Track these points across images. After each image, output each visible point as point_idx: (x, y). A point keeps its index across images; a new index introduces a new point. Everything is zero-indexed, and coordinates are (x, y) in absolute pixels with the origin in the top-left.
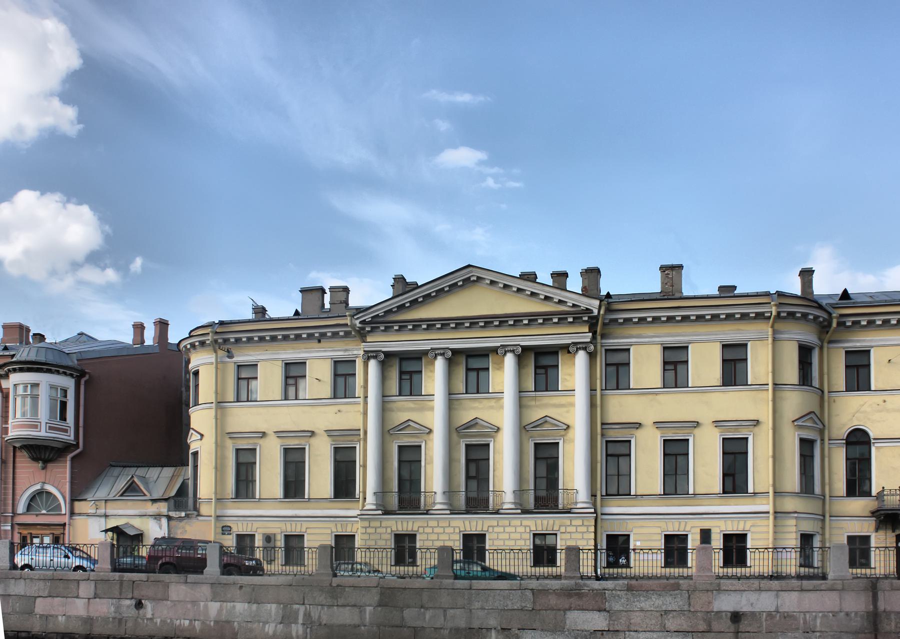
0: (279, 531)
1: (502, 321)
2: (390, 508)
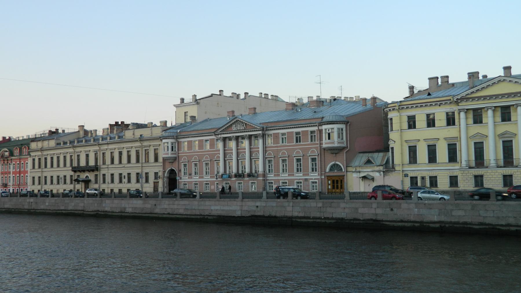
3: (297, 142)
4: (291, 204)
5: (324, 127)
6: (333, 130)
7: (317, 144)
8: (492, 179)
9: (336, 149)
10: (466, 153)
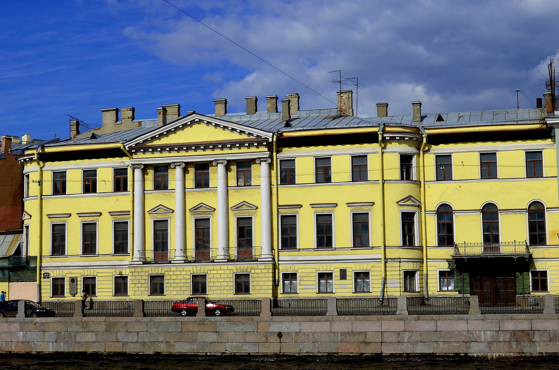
0: (80, 275)
1: (215, 145)
2: (148, 260)
8: (176, 281)
10: (140, 239)
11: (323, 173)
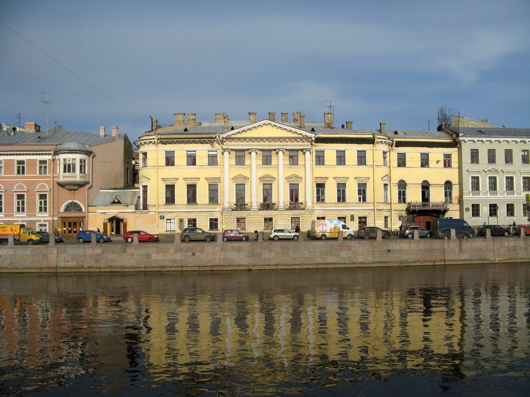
1: (279, 139)
3: (19, 173)
4: (55, 251)
5: (62, 157)
6: (74, 161)
7: (49, 177)
9: (71, 184)
10: (228, 197)
11: (341, 159)
